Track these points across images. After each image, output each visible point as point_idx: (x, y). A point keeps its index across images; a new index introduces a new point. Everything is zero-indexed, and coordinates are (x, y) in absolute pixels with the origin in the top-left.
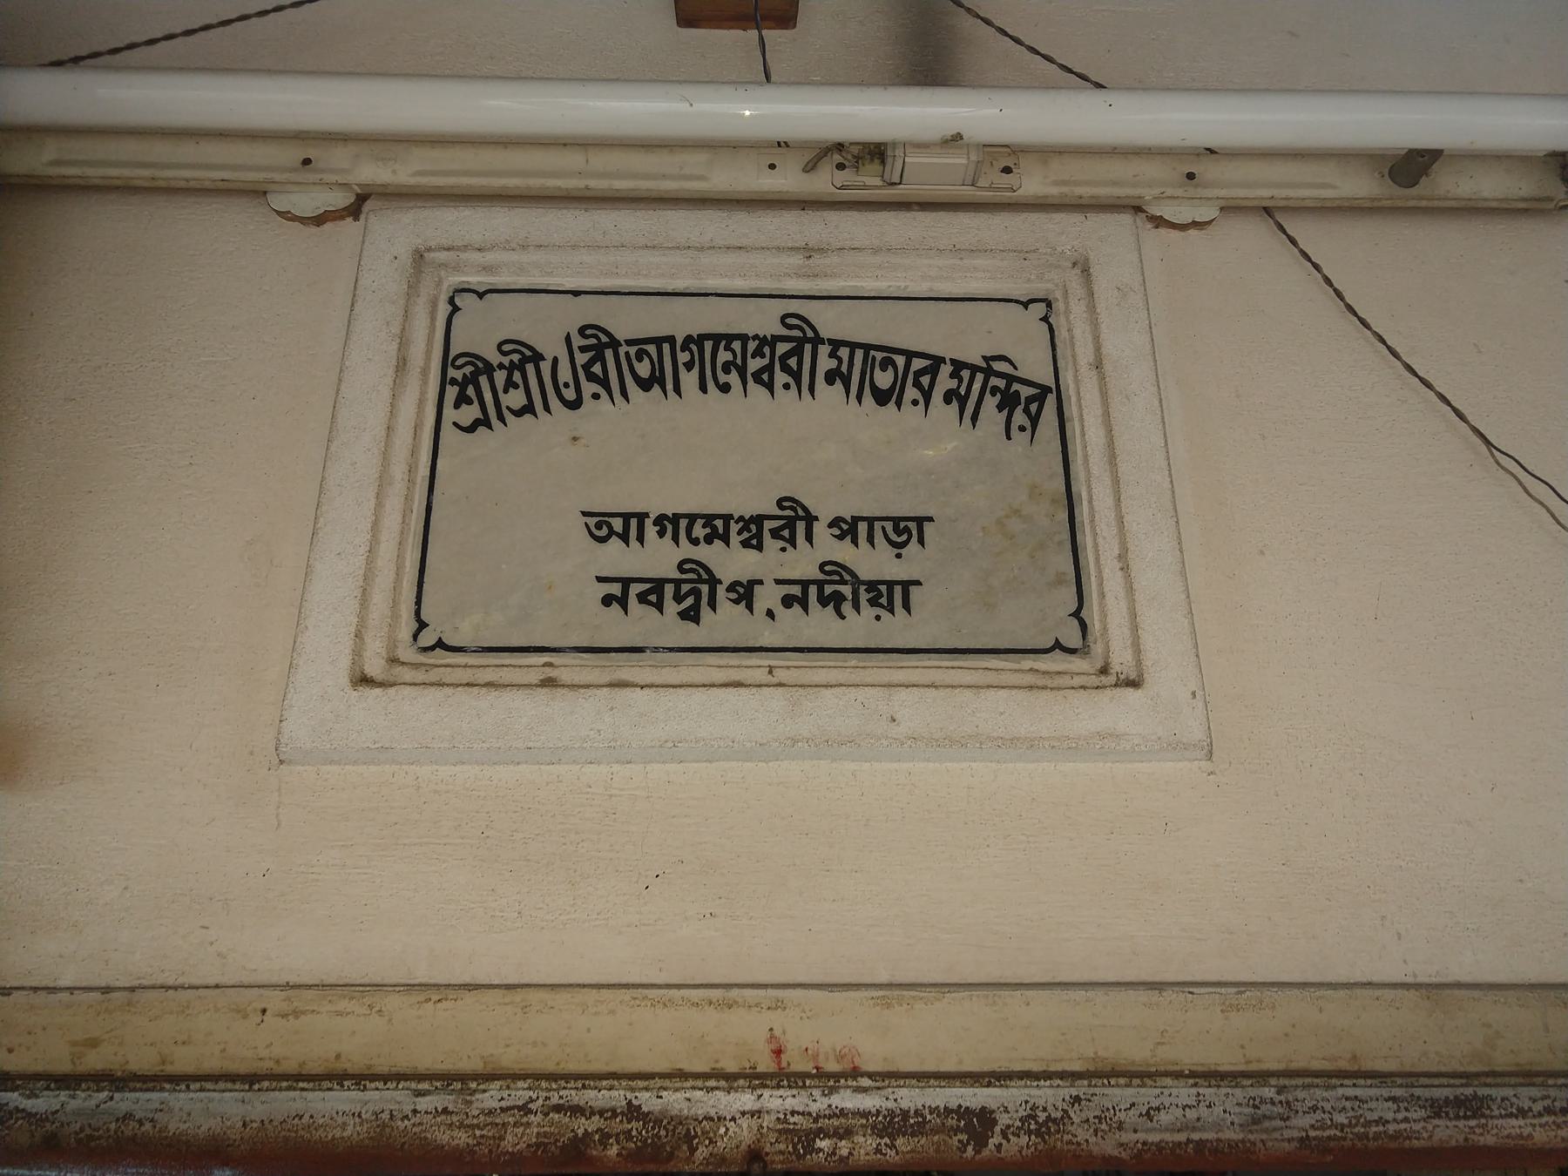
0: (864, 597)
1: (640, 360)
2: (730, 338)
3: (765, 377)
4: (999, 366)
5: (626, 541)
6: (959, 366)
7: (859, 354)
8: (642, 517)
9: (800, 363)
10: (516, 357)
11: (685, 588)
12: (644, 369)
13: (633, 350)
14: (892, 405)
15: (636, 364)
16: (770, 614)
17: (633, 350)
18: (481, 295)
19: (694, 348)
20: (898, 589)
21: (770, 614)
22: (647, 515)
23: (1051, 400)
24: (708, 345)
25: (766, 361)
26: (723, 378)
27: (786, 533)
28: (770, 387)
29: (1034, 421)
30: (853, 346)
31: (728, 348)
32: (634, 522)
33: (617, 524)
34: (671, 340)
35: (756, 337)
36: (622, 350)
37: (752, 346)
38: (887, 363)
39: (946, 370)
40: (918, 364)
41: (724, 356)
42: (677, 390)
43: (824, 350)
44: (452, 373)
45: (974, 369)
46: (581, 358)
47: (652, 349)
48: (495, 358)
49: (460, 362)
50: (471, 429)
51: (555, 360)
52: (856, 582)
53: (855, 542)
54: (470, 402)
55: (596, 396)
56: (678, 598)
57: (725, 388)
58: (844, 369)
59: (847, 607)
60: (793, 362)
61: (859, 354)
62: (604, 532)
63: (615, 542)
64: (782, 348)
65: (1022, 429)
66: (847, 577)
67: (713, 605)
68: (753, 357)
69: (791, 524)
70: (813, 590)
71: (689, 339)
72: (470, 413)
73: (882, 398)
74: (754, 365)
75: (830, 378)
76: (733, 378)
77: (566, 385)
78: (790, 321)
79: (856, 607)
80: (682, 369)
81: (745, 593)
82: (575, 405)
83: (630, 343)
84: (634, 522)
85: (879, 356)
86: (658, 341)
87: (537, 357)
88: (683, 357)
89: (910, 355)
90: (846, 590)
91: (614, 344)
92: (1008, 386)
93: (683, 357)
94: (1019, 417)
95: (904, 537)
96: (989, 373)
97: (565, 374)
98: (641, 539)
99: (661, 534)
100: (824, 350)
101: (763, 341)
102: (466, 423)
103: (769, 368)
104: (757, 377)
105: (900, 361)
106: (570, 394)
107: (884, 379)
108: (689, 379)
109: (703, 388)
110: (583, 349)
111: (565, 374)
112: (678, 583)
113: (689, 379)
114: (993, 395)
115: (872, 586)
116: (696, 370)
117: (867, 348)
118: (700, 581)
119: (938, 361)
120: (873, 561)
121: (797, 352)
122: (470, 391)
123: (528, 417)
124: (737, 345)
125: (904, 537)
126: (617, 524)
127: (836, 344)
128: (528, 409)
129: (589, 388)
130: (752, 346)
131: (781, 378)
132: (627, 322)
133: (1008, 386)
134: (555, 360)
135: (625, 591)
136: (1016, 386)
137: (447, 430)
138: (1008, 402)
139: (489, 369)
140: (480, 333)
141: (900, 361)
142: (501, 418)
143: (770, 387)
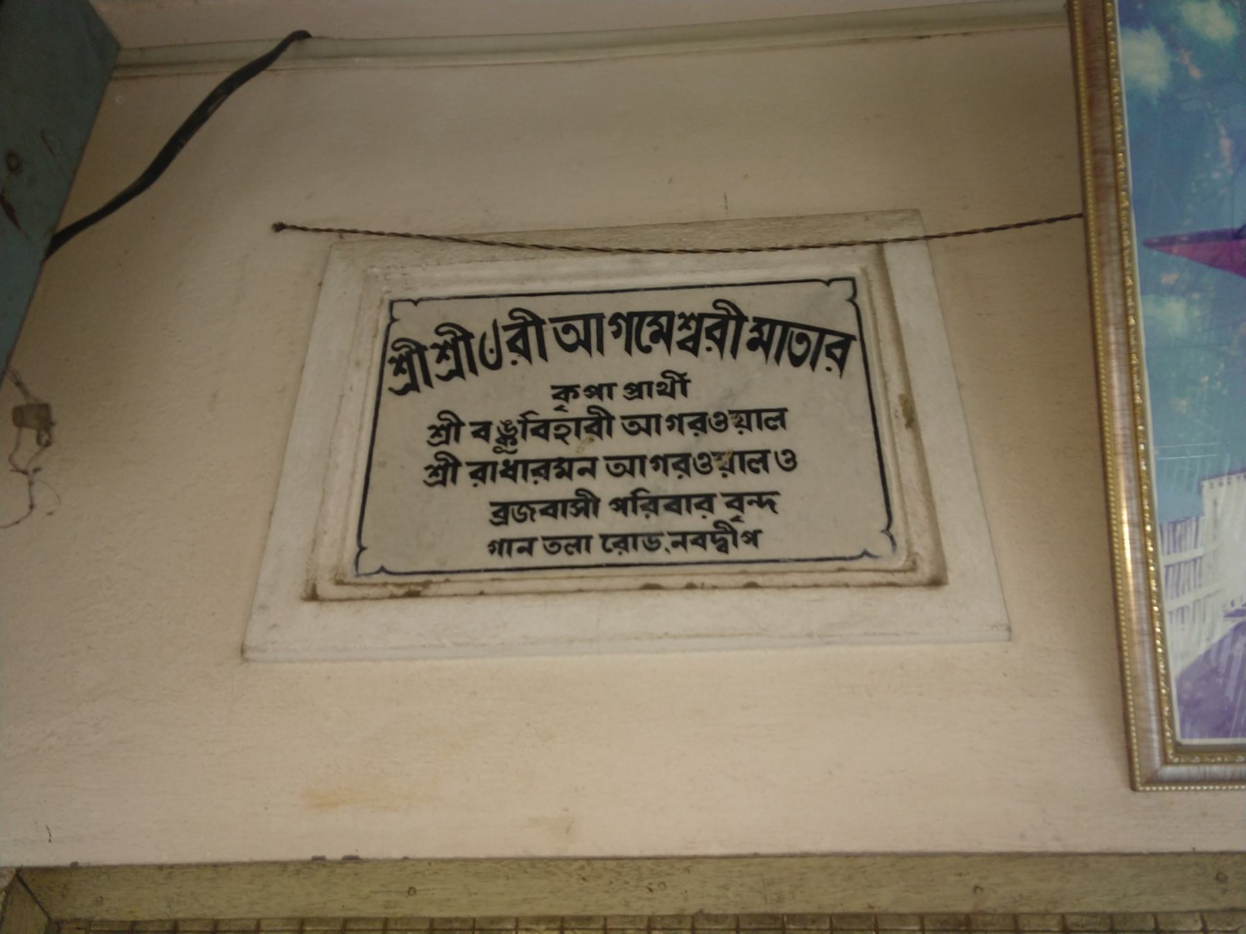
7: (779, 329)
8: (658, 417)
9: (724, 334)
10: (448, 338)
17: (559, 326)
19: (623, 324)
25: (692, 332)
27: (595, 429)
28: (695, 351)
30: (773, 323)
32: (653, 421)
33: (642, 422)
35: (682, 315)
37: (678, 322)
38: (802, 338)
40: (829, 339)
43: (747, 326)
47: (579, 325)
50: (402, 392)
54: (404, 372)
56: (714, 541)
58: (765, 338)
61: (779, 329)
62: (635, 428)
63: (642, 434)
64: (708, 323)
67: (735, 544)
68: (680, 329)
69: (598, 422)
72: (404, 379)
73: (796, 361)
75: (752, 345)
77: (491, 351)
78: (720, 305)
82: (497, 365)
84: (653, 421)
85: (797, 331)
86: (586, 318)
87: (467, 336)
89: (823, 332)
97: (490, 343)
98: (658, 431)
99: (670, 428)
103: (695, 338)
104: (682, 345)
105: (813, 336)
107: (799, 349)
109: (628, 349)
110: (506, 328)
111: (490, 343)
112: (713, 534)
116: (623, 336)
117: (786, 325)
122: (405, 366)
123: (412, 394)
126: (642, 422)
127: (760, 322)
129: (508, 356)
131: (705, 342)
139: (421, 349)
140: (419, 328)
142: (428, 382)
143: (695, 351)
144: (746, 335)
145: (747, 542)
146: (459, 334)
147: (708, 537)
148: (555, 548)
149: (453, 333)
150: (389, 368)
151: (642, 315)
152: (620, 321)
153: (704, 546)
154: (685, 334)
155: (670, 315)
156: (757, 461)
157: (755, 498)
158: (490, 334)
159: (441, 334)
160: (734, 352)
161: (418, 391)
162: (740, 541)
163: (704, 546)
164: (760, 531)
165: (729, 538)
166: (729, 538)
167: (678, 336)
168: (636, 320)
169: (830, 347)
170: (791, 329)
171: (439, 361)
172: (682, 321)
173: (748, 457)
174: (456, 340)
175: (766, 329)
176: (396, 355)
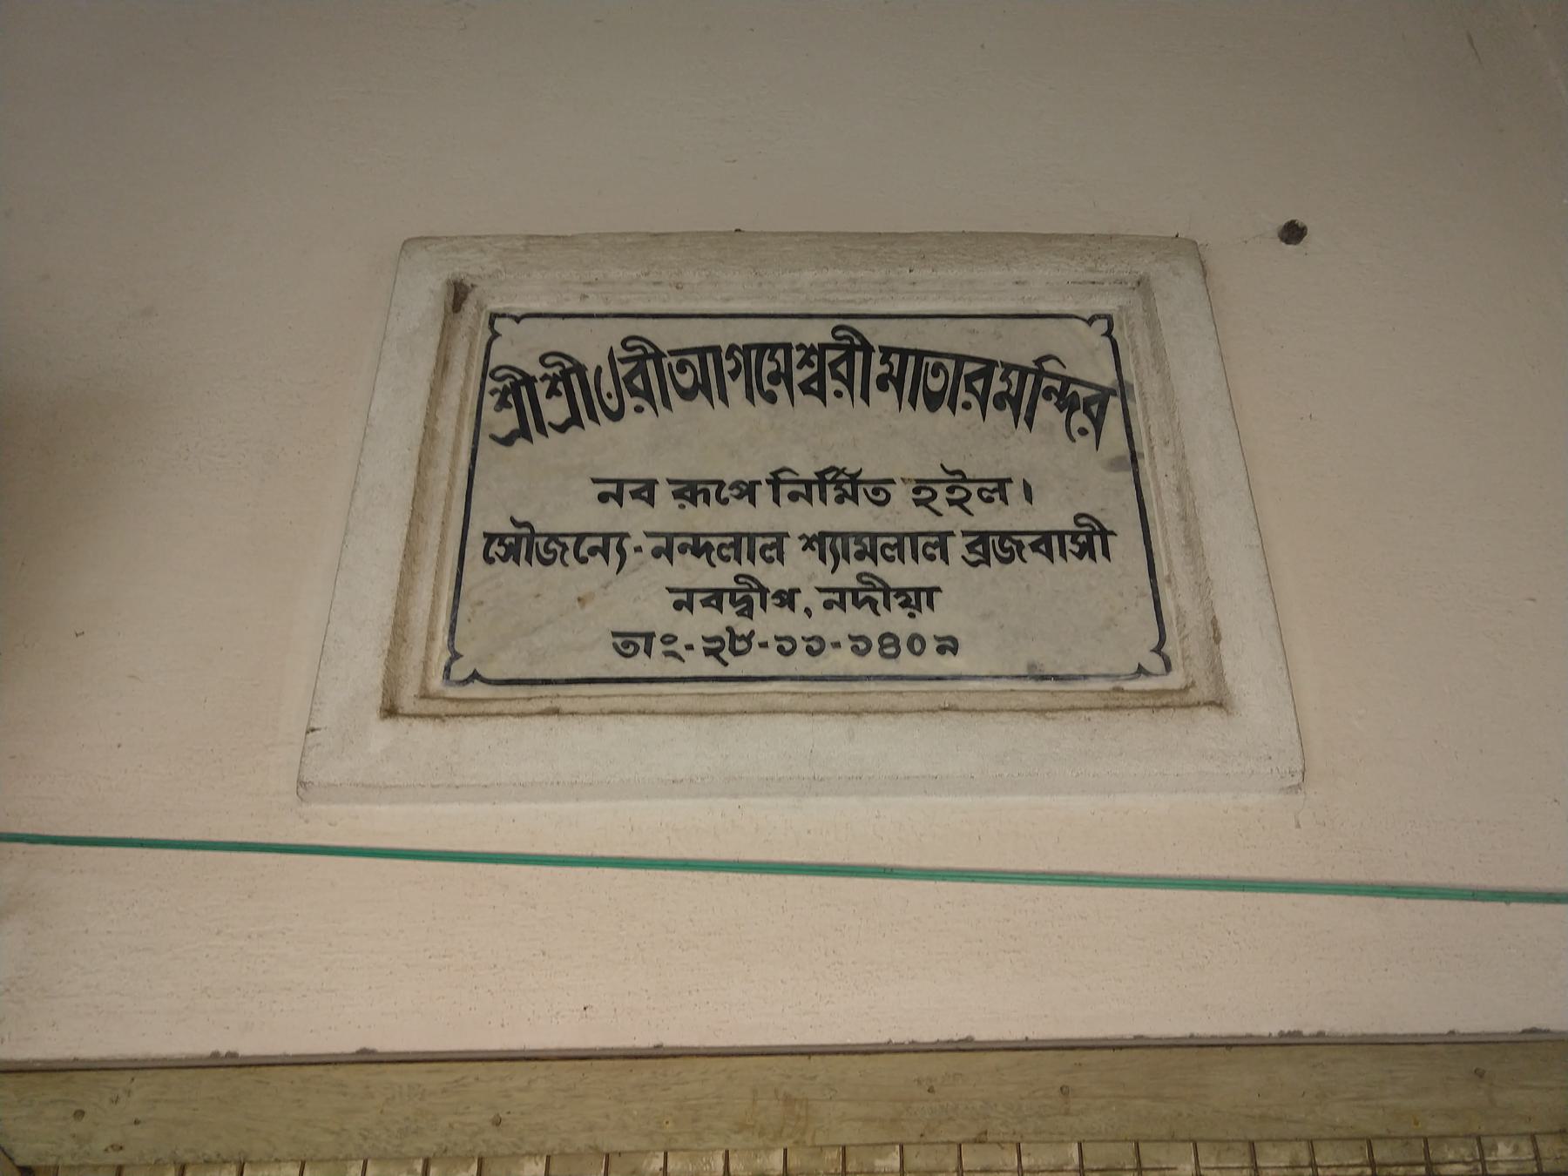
0: (894, 602)
1: (683, 371)
2: (774, 347)
3: (815, 386)
4: (1050, 366)
5: (810, 500)
6: (1009, 368)
7: (912, 359)
11: (739, 596)
12: (686, 380)
13: (674, 360)
14: (944, 409)
15: (678, 376)
16: (807, 611)
17: (674, 360)
18: (518, 320)
20: (924, 596)
21: (807, 611)
22: (653, 635)
23: (1114, 403)
24: (754, 353)
25: (815, 370)
26: (767, 386)
28: (821, 395)
29: (1098, 423)
30: (904, 353)
31: (771, 358)
34: (716, 350)
35: (801, 347)
36: (665, 362)
37: (797, 356)
39: (998, 372)
40: (969, 368)
41: (768, 367)
42: (724, 398)
43: (876, 357)
44: (491, 384)
45: (1024, 372)
46: (623, 370)
47: (694, 359)
48: (537, 371)
49: (499, 374)
50: (508, 441)
51: (599, 370)
52: (886, 590)
53: (1093, 557)
55: (639, 409)
56: (733, 602)
57: (771, 398)
58: (895, 373)
59: (881, 607)
60: (842, 369)
61: (912, 359)
64: (831, 355)
65: (1083, 432)
66: (878, 585)
67: (763, 606)
68: (800, 366)
70: (849, 597)
71: (732, 348)
74: (799, 376)
75: (882, 385)
76: (781, 390)
79: (888, 606)
80: (727, 378)
81: (787, 598)
82: (616, 416)
83: (673, 353)
85: (931, 361)
86: (701, 352)
87: (580, 369)
88: (729, 365)
89: (960, 360)
90: (879, 596)
91: (658, 356)
92: (1065, 388)
93: (729, 365)
94: (1080, 420)
95: (551, 556)
96: (1040, 373)
97: (607, 384)
100: (876, 357)
101: (811, 350)
102: (502, 432)
103: (819, 377)
104: (805, 388)
106: (613, 404)
107: (935, 384)
108: (736, 388)
109: (750, 397)
111: (607, 384)
112: (733, 592)
113: (736, 388)
114: (1048, 398)
115: (900, 592)
116: (742, 376)
117: (920, 355)
118: (751, 589)
119: (990, 364)
120: (899, 574)
121: (849, 358)
124: (780, 355)
125: (551, 556)
127: (887, 352)
128: (575, 420)
130: (797, 356)
131: (832, 385)
132: (667, 337)
133: (1065, 388)
134: (599, 370)
135: (691, 599)
136: (1073, 388)
137: (484, 439)
138: (1068, 404)
139: (529, 381)
140: (520, 350)
141: (950, 365)
143: (821, 395)
144: (877, 369)
145: (781, 606)
146: (568, 365)
147: (726, 596)
148: (631, 649)
149: (560, 364)
150: (490, 401)
151: (762, 348)
152: (737, 354)
153: (720, 608)
154: (808, 372)
155: (787, 348)
156: (892, 547)
157: (1057, 384)
158: (606, 370)
159: (547, 366)
160: (865, 396)
161: (531, 441)
162: (770, 602)
163: (720, 608)
164: (799, 591)
165: (756, 597)
166: (756, 597)
167: (799, 376)
168: (754, 353)
169: (970, 379)
170: (926, 360)
171: (548, 396)
172: (803, 353)
173: (881, 541)
174: (567, 374)
175: (895, 359)
176: (500, 386)
